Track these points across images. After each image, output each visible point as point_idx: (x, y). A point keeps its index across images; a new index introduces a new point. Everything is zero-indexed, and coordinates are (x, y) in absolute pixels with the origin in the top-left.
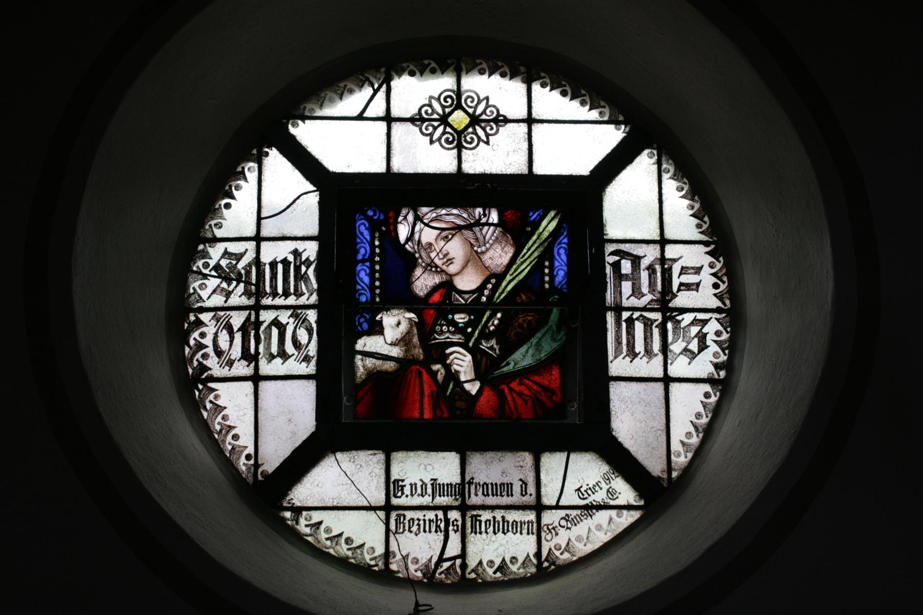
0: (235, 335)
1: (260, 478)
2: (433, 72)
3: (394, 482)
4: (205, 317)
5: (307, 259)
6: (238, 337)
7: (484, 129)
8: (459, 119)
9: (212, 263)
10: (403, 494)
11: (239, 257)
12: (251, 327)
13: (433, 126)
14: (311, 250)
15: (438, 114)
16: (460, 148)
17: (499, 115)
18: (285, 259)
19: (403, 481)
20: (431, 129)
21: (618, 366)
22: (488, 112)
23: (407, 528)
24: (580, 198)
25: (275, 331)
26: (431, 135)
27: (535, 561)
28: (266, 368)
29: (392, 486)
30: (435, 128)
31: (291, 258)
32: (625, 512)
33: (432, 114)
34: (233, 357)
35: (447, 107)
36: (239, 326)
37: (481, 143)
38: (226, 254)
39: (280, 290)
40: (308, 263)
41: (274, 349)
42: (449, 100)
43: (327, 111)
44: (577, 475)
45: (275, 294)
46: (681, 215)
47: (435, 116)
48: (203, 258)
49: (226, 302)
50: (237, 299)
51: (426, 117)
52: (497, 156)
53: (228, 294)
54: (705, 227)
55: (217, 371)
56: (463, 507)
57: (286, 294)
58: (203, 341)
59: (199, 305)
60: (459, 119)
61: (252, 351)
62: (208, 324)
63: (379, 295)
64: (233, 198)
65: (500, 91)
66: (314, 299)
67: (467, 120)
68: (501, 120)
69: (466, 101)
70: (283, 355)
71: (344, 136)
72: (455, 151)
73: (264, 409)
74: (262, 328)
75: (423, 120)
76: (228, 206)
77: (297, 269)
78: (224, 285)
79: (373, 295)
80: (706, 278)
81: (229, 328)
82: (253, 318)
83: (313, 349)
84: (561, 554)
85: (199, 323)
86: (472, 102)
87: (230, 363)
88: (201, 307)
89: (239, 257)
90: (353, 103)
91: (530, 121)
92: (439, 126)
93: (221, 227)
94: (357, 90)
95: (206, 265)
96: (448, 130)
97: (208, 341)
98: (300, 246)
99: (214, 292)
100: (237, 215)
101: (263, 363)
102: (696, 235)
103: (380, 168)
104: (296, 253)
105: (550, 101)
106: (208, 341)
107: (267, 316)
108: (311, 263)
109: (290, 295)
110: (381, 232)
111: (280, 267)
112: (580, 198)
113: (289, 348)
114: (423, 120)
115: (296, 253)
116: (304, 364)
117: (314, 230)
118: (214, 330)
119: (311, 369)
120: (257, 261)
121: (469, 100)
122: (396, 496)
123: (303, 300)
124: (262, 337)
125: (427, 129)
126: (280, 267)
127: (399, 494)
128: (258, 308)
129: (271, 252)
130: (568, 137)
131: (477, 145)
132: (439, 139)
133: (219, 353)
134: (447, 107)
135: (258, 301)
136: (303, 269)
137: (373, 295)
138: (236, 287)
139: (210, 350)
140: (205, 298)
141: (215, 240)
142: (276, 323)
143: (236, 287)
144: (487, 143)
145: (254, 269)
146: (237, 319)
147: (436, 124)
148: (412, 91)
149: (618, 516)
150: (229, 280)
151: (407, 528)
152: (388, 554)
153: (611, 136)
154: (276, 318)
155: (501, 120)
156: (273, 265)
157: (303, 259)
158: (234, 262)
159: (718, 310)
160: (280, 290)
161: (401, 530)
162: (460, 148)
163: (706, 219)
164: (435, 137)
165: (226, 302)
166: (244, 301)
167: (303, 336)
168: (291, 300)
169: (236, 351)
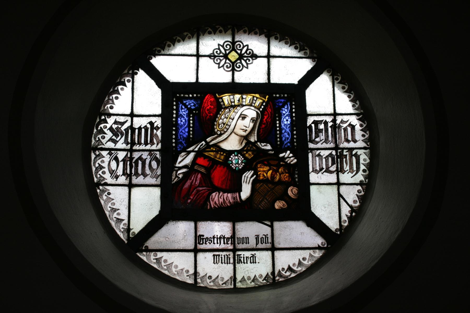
0: (120, 163)
1: (131, 236)
2: (221, 32)
3: (199, 236)
4: (104, 153)
5: (157, 126)
6: (121, 164)
7: (245, 61)
8: (233, 56)
9: (108, 126)
10: (203, 243)
11: (123, 124)
12: (128, 160)
13: (220, 59)
14: (158, 122)
15: (223, 53)
16: (233, 70)
17: (214, 59)
18: (146, 126)
19: (203, 236)
20: (219, 61)
21: (313, 178)
22: (248, 52)
23: (204, 242)
24: (295, 94)
25: (140, 162)
26: (219, 64)
27: (272, 277)
28: (135, 180)
29: (199, 238)
30: (221, 60)
31: (149, 126)
32: (317, 251)
33: (247, 59)
34: (118, 174)
35: (227, 50)
36: (122, 158)
37: (244, 68)
38: (116, 122)
39: (143, 141)
40: (157, 128)
41: (140, 171)
42: (228, 46)
43: (166, 52)
44: (294, 232)
45: (140, 143)
46: (345, 104)
47: (221, 55)
48: (104, 123)
49: (115, 146)
50: (121, 145)
51: (217, 55)
52: (253, 73)
53: (115, 142)
54: (357, 106)
55: (108, 178)
56: (234, 249)
57: (146, 144)
58: (103, 165)
59: (101, 146)
60: (233, 56)
61: (128, 172)
62: (106, 156)
63: (192, 120)
64: (119, 94)
65: (257, 45)
66: (159, 146)
67: (237, 56)
68: (254, 56)
69: (237, 46)
70: (145, 175)
71: (177, 65)
72: (231, 73)
73: (135, 204)
74: (134, 161)
75: (215, 56)
76: (117, 98)
77: (152, 131)
78: (114, 137)
79: (189, 134)
80: (359, 134)
81: (116, 159)
82: (129, 155)
83: (159, 172)
84: (285, 272)
85: (100, 156)
86: (239, 47)
87: (117, 177)
88: (102, 148)
89: (123, 124)
90: (180, 48)
91: (198, 56)
92: (244, 54)
93: (166, 260)
94: (182, 41)
95: (106, 127)
96: (228, 61)
97: (105, 165)
98: (153, 119)
99: (109, 141)
100: (120, 104)
101: (134, 178)
102: (352, 111)
103: (194, 80)
104: (151, 123)
105: (278, 48)
106: (105, 165)
107: (136, 155)
108: (159, 128)
109: (148, 144)
110: (193, 114)
111: (143, 130)
112: (295, 94)
113: (148, 171)
114: (215, 56)
115: (151, 123)
116: (155, 179)
117: (159, 112)
118: (109, 160)
119: (158, 182)
120: (131, 127)
121: (229, 66)
122: (199, 244)
123: (154, 147)
124: (134, 164)
125: (217, 61)
126: (143, 130)
127: (201, 243)
128: (131, 151)
129: (138, 122)
130: (289, 67)
131: (242, 69)
132: (223, 66)
133: (112, 172)
134: (227, 50)
135: (132, 147)
136: (155, 131)
137: (189, 134)
138: (120, 139)
139: (106, 170)
140: (104, 143)
141: (110, 115)
142: (140, 158)
143: (120, 139)
144: (247, 68)
145: (130, 131)
146: (121, 155)
147: (221, 58)
148: (210, 44)
149: (314, 252)
150: (117, 136)
151: (204, 242)
152: (196, 273)
153: (306, 65)
154: (141, 156)
155: (254, 56)
156: (140, 129)
157: (155, 126)
158: (120, 126)
159: (364, 148)
160: (143, 141)
161: (201, 243)
162: (233, 70)
163: (358, 102)
164: (221, 65)
165: (115, 146)
166: (124, 146)
167: (154, 164)
168: (148, 147)
169: (120, 171)
